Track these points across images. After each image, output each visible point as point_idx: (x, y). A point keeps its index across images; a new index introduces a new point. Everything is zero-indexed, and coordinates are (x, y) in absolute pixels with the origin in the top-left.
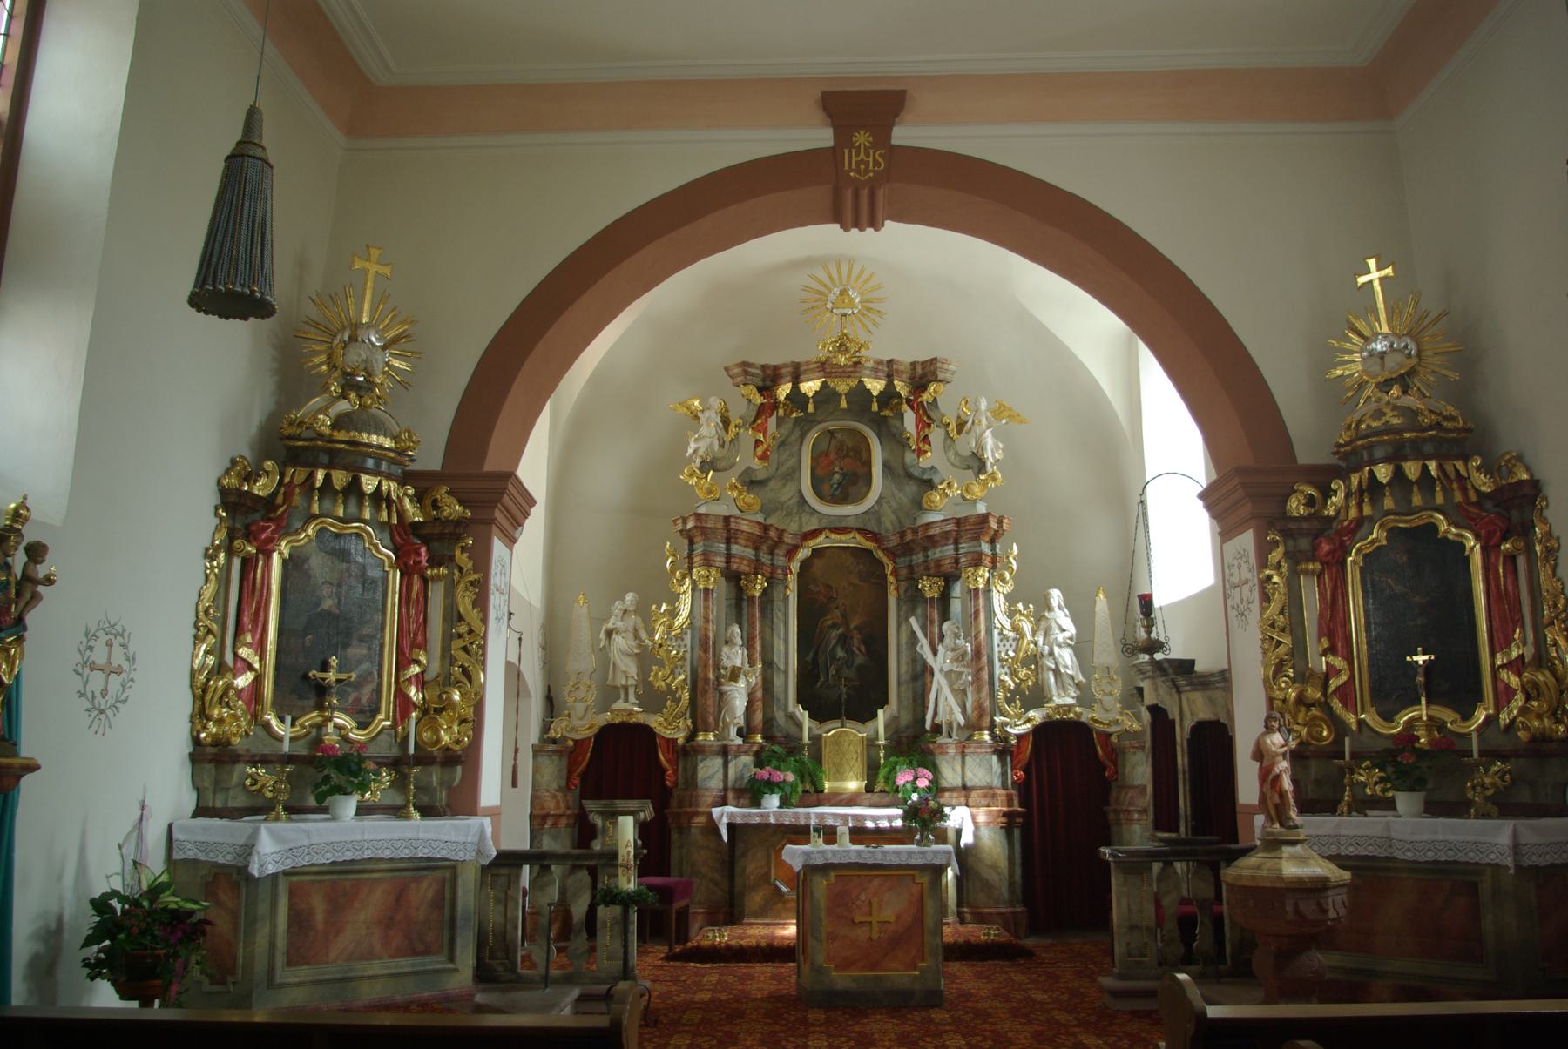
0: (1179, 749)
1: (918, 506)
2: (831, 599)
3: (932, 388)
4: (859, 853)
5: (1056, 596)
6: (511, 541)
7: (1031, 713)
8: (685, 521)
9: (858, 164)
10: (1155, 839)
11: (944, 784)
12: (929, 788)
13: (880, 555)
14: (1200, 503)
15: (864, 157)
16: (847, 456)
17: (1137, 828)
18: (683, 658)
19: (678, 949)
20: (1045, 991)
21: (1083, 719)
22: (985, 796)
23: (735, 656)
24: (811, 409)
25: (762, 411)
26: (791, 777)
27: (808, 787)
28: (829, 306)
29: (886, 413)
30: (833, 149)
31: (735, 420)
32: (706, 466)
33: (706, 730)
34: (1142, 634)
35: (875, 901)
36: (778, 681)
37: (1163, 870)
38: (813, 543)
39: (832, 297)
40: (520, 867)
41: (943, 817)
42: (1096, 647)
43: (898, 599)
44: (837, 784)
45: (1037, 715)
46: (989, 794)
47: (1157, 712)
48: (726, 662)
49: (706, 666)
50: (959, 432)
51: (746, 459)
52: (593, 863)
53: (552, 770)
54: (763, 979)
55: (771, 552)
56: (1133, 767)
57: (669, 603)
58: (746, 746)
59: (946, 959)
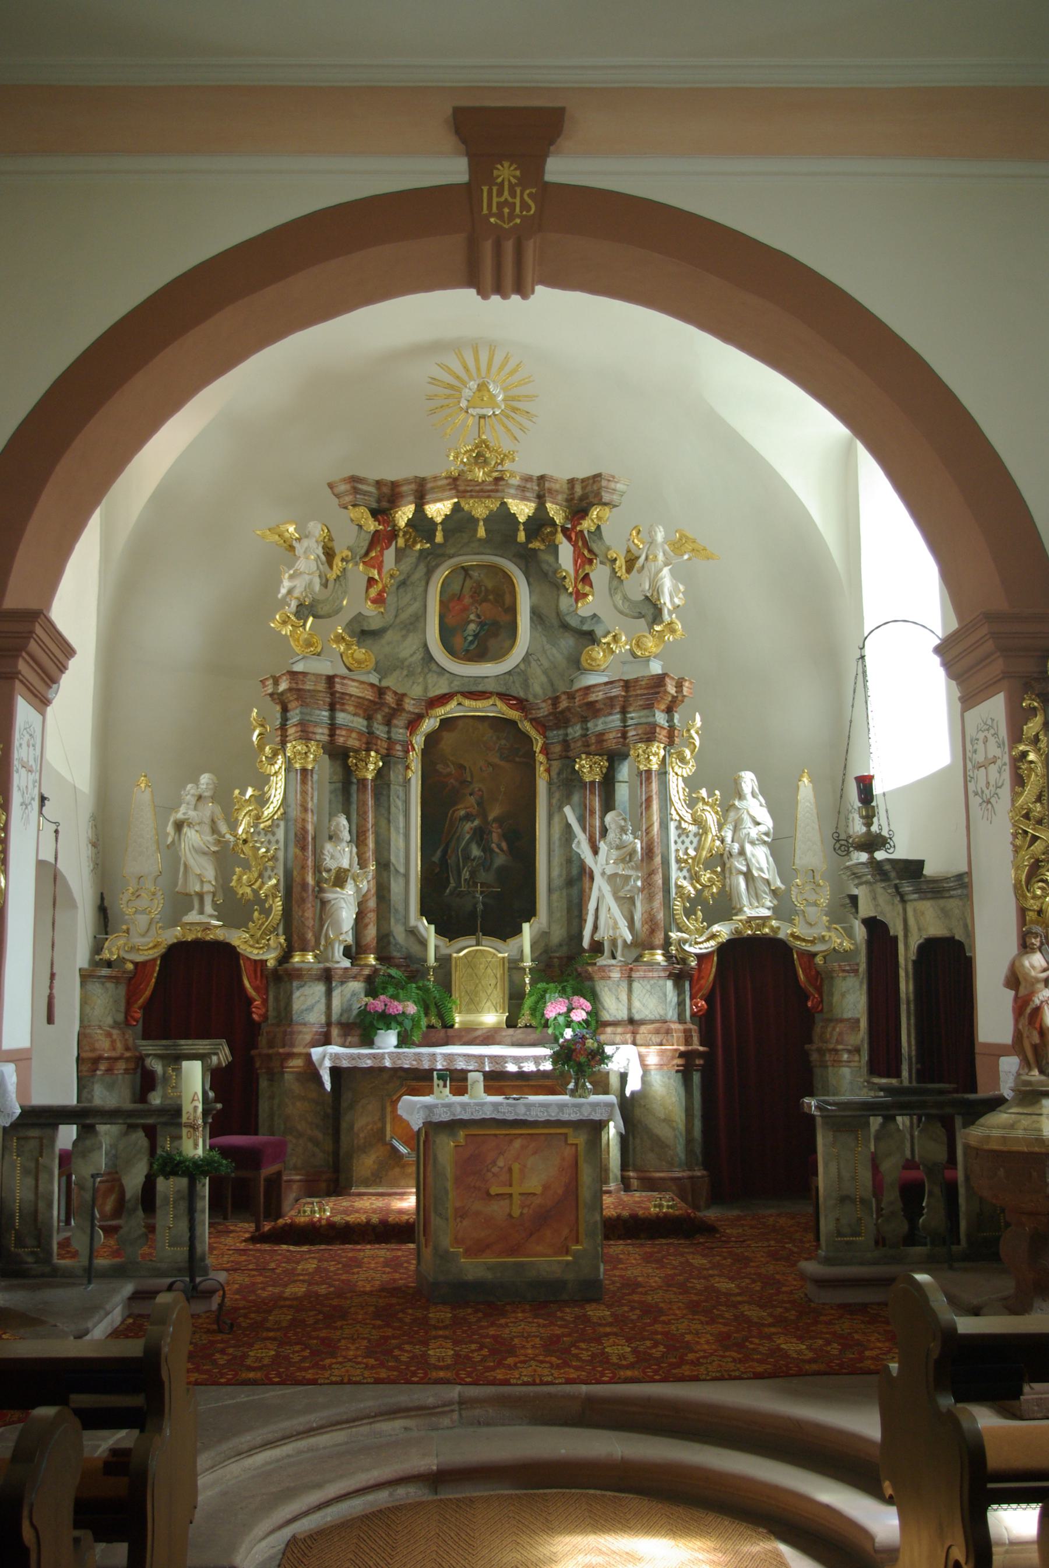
0: (902, 973)
1: (576, 664)
2: (464, 783)
3: (594, 513)
4: (496, 1105)
5: (749, 780)
6: (42, 702)
7: (716, 928)
8: (276, 682)
9: (500, 206)
10: (872, 1086)
11: (606, 1017)
12: (586, 1021)
13: (527, 727)
14: (937, 660)
15: (507, 199)
16: (485, 600)
17: (846, 1071)
18: (274, 858)
19: (267, 1227)
20: (732, 1279)
21: (781, 935)
22: (657, 1032)
23: (341, 855)
24: (439, 538)
25: (376, 540)
26: (412, 1008)
27: (434, 1020)
28: (463, 404)
29: (535, 545)
30: (468, 186)
31: (341, 551)
32: (304, 610)
33: (304, 950)
34: (858, 828)
35: (516, 1167)
36: (396, 887)
37: (883, 1126)
38: (442, 712)
39: (467, 393)
40: (55, 1127)
41: (604, 1058)
42: (799, 845)
43: (550, 783)
44: (471, 1017)
45: (723, 931)
46: (661, 1027)
47: (873, 925)
48: (329, 863)
49: (303, 867)
50: (629, 570)
51: (356, 602)
52: (150, 1121)
53: (106, 1002)
54: (374, 1264)
55: (388, 723)
56: (843, 995)
57: (256, 787)
58: (355, 970)
59: (607, 1237)
